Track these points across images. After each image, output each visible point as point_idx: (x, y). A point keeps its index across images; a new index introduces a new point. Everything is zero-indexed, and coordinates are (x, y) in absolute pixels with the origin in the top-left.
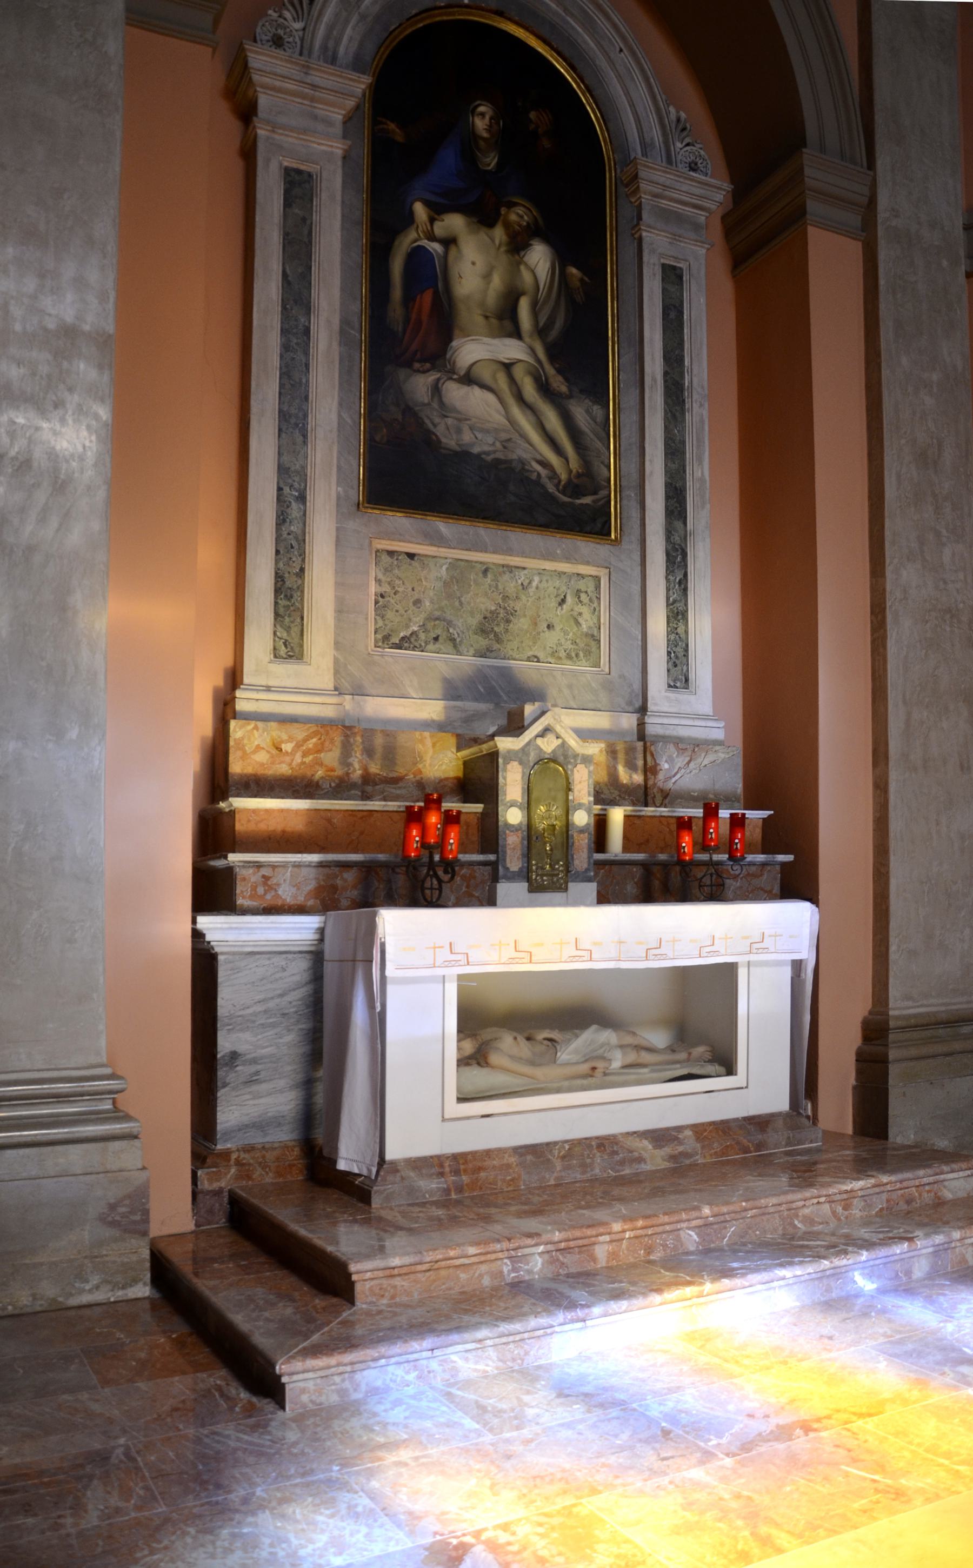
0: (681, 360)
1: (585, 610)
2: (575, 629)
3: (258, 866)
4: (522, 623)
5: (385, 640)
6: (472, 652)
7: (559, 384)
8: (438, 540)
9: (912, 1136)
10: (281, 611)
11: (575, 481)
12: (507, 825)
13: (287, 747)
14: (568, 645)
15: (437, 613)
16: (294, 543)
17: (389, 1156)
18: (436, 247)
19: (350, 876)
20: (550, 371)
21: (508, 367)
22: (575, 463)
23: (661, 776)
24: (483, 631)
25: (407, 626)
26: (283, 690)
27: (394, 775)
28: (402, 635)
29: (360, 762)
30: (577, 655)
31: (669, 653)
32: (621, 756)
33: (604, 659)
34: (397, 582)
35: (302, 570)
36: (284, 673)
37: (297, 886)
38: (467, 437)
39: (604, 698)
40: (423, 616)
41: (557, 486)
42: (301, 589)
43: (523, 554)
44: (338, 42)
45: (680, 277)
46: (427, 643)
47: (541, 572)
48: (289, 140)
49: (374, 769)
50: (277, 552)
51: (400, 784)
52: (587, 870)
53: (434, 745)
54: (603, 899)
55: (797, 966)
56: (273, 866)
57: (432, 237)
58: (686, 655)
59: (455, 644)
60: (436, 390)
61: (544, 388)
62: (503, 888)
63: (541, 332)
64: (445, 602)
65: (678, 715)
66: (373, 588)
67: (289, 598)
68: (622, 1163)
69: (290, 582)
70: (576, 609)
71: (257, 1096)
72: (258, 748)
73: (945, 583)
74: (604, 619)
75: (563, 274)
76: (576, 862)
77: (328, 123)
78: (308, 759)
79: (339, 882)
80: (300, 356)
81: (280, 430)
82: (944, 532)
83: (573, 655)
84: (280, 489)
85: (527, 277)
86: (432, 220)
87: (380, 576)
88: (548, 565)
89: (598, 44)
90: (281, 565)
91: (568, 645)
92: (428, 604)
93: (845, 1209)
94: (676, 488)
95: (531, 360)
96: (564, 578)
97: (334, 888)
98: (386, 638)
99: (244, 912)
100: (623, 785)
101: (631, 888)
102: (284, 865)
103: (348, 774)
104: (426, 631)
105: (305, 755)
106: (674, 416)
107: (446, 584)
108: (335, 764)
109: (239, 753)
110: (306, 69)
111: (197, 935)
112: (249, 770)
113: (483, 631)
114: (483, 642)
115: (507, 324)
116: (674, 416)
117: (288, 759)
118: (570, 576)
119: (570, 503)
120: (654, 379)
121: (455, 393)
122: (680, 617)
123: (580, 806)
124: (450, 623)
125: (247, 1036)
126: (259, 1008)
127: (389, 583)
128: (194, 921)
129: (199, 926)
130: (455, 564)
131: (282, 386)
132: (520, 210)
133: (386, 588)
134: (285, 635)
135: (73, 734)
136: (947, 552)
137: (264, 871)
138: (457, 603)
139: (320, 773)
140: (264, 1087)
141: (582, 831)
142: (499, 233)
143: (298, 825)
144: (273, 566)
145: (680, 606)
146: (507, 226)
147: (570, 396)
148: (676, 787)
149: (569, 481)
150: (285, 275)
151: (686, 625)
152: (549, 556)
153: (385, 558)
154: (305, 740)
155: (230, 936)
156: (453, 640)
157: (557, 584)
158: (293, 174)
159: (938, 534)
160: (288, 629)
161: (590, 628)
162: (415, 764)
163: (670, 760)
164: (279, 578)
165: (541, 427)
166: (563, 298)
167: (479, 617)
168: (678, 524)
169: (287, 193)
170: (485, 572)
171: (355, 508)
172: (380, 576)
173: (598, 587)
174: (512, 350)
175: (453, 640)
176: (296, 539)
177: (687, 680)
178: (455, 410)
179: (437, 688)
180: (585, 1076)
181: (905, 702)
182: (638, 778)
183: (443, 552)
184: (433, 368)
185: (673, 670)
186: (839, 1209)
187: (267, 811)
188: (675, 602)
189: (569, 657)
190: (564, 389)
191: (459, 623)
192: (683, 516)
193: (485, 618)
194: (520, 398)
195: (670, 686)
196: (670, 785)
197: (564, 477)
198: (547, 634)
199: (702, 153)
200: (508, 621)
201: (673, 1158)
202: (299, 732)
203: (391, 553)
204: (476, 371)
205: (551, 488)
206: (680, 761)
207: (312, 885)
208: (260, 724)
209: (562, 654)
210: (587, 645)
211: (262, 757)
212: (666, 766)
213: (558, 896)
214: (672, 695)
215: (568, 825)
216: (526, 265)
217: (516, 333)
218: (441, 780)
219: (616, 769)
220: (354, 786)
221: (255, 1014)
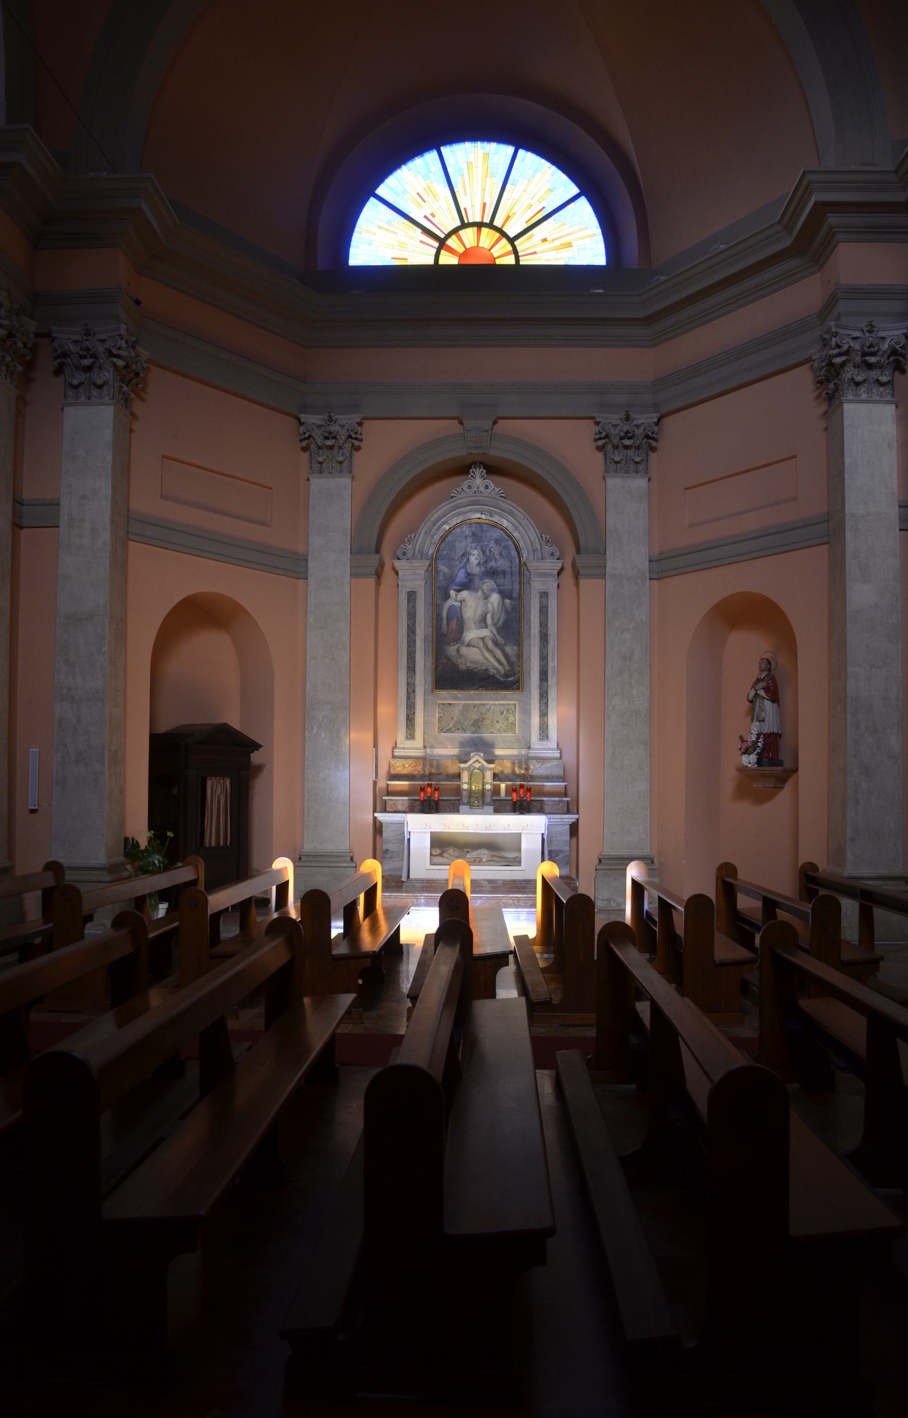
1: (511, 716)
2: (507, 722)
3: (392, 800)
4: (488, 722)
5: (441, 730)
6: (470, 732)
7: (501, 640)
8: (458, 699)
9: (606, 896)
10: (408, 725)
11: (507, 673)
12: (463, 789)
13: (406, 766)
14: (504, 727)
15: (458, 721)
16: (412, 705)
17: (411, 877)
19: (418, 803)
20: (498, 637)
21: (483, 639)
22: (507, 667)
23: (530, 771)
24: (474, 725)
25: (449, 726)
26: (408, 749)
27: (439, 772)
28: (447, 728)
29: (429, 769)
30: (507, 730)
31: (540, 728)
32: (517, 764)
34: (445, 713)
35: (414, 713)
36: (409, 744)
40: (454, 722)
41: (500, 676)
42: (414, 718)
43: (486, 700)
44: (424, 547)
45: (548, 595)
46: (455, 730)
47: (494, 705)
49: (433, 771)
50: (407, 708)
51: (441, 775)
52: (490, 802)
53: (452, 763)
55: (543, 834)
56: (396, 800)
58: (547, 728)
59: (464, 730)
60: (458, 650)
61: (496, 643)
62: (461, 808)
63: (495, 625)
64: (461, 718)
65: (543, 749)
66: (437, 715)
67: (410, 721)
68: (476, 886)
69: (411, 716)
70: (507, 715)
72: (398, 766)
73: (633, 702)
75: (503, 604)
76: (486, 800)
78: (413, 769)
79: (415, 805)
80: (413, 649)
81: (407, 672)
83: (506, 730)
84: (407, 690)
85: (490, 606)
87: (440, 711)
88: (497, 702)
90: (408, 712)
91: (504, 727)
92: (455, 718)
93: (518, 902)
94: (544, 671)
95: (491, 635)
96: (503, 706)
97: (414, 806)
98: (442, 730)
99: (388, 812)
100: (517, 774)
101: (508, 808)
102: (399, 800)
103: (424, 773)
104: (455, 727)
105: (411, 768)
106: (544, 646)
107: (461, 712)
108: (421, 770)
109: (393, 768)
110: (411, 563)
111: (375, 819)
112: (396, 772)
113: (474, 725)
114: (474, 729)
115: (483, 624)
116: (544, 646)
117: (406, 769)
118: (505, 705)
119: (504, 681)
120: (535, 634)
121: (464, 650)
122: (545, 715)
123: (488, 783)
124: (463, 724)
125: (390, 845)
126: (394, 838)
127: (443, 713)
128: (373, 815)
129: (375, 816)
130: (464, 705)
131: (408, 658)
133: (442, 715)
134: (409, 732)
135: (341, 768)
136: (635, 691)
137: (394, 801)
138: (465, 718)
139: (416, 773)
141: (488, 790)
143: (406, 788)
144: (406, 712)
145: (545, 712)
147: (506, 645)
148: (535, 774)
150: (408, 625)
151: (548, 718)
153: (441, 706)
154: (412, 763)
155: (384, 818)
156: (463, 729)
157: (500, 708)
158: (410, 593)
160: (410, 730)
161: (512, 721)
162: (445, 769)
163: (534, 765)
164: (408, 715)
165: (495, 657)
166: (503, 612)
167: (472, 721)
170: (475, 706)
171: (431, 692)
172: (440, 711)
173: (515, 707)
174: (485, 633)
175: (463, 729)
176: (413, 704)
177: (547, 736)
179: (457, 745)
180: (473, 862)
182: (523, 772)
183: (460, 702)
184: (457, 643)
185: (542, 734)
186: (516, 902)
187: (398, 785)
188: (543, 710)
189: (505, 731)
190: (503, 642)
191: (466, 723)
192: (547, 680)
193: (475, 721)
195: (540, 739)
196: (534, 773)
199: (555, 548)
200: (483, 721)
201: (493, 887)
202: (410, 761)
203: (443, 704)
205: (498, 677)
206: (538, 766)
207: (407, 805)
208: (399, 760)
209: (502, 730)
210: (511, 727)
211: (399, 769)
212: (533, 767)
213: (480, 811)
215: (483, 789)
216: (490, 603)
217: (486, 627)
218: (454, 774)
219: (514, 768)
220: (426, 776)
221: (392, 839)
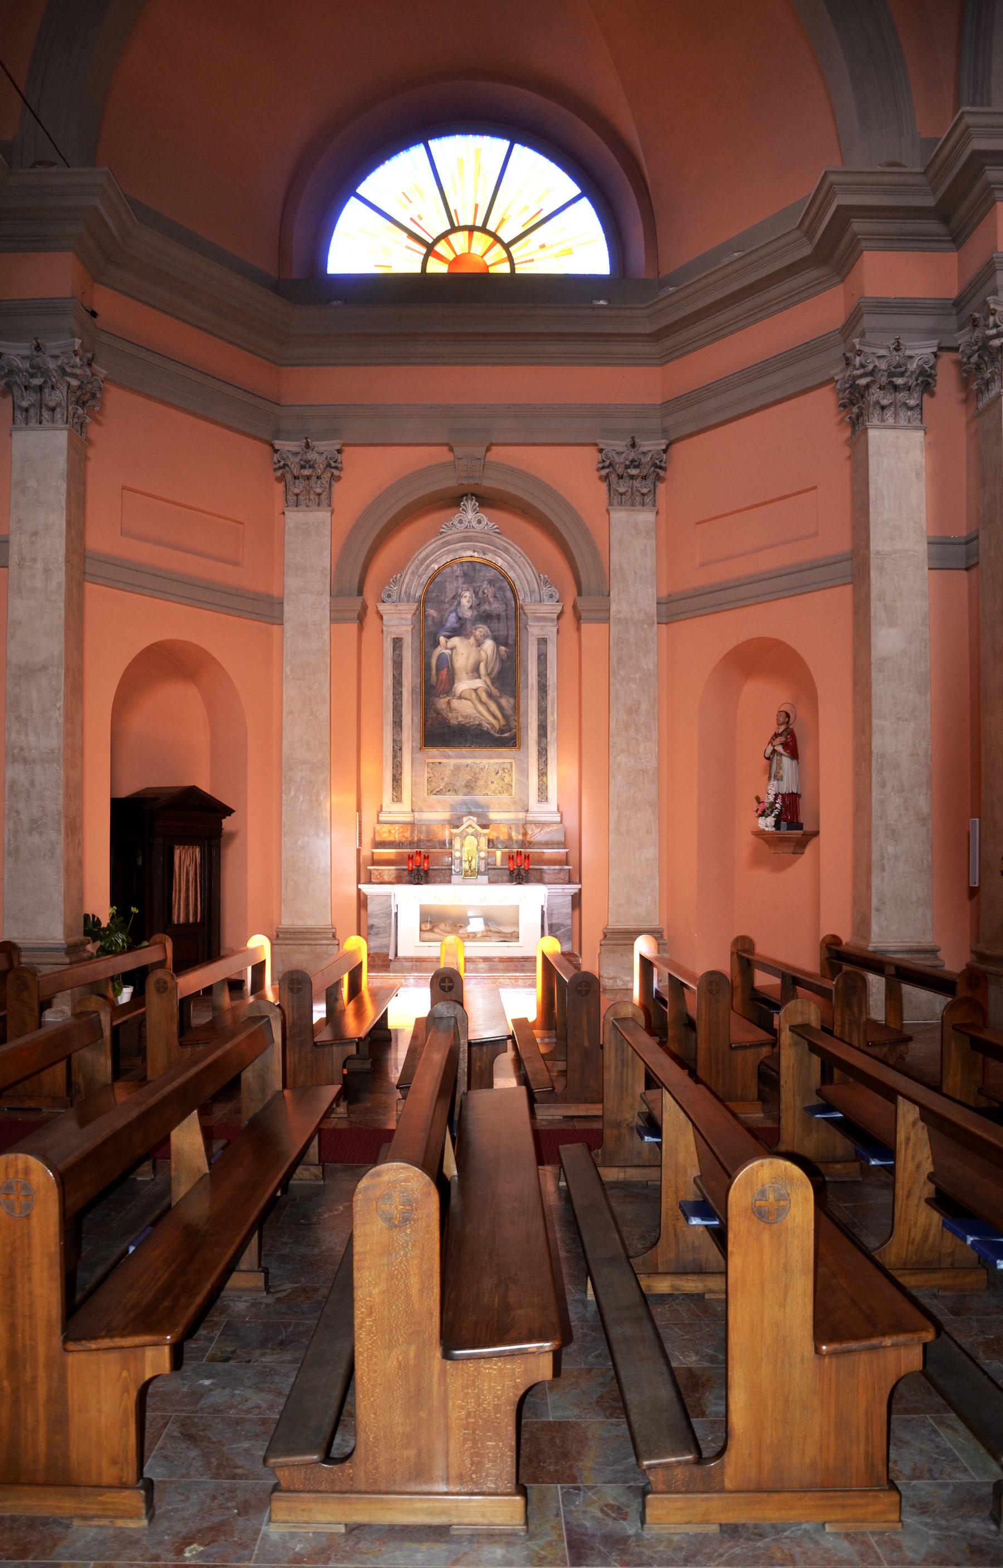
0: (546, 675)
1: (507, 776)
3: (378, 870)
4: (481, 783)
5: (431, 792)
7: (495, 692)
13: (393, 832)
14: (500, 789)
18: (448, 652)
19: (406, 873)
20: (492, 688)
21: (475, 690)
22: (502, 722)
23: (528, 836)
24: (466, 786)
33: (513, 793)
36: (396, 807)
37: (390, 876)
38: (460, 719)
39: (512, 807)
42: (401, 779)
44: (410, 588)
45: (546, 642)
48: (394, 629)
54: (491, 882)
55: (542, 907)
57: (447, 648)
60: (449, 703)
61: (490, 695)
63: (489, 675)
65: (541, 812)
66: (426, 775)
71: (379, 938)
74: (514, 778)
75: (498, 651)
77: (406, 619)
80: (399, 702)
82: (641, 739)
85: (483, 654)
86: (447, 642)
89: (511, 558)
91: (500, 789)
95: (485, 686)
99: (374, 883)
111: (359, 891)
112: (382, 839)
113: (466, 786)
114: (466, 790)
115: (476, 675)
121: (455, 703)
124: (454, 785)
125: (376, 920)
132: (480, 629)
133: (431, 775)
136: (641, 748)
140: (381, 935)
142: (472, 640)
143: (393, 857)
146: (475, 637)
147: (501, 697)
149: (500, 728)
150: (394, 675)
152: (490, 758)
159: (637, 740)
163: (532, 830)
164: (394, 776)
167: (465, 782)
168: (544, 740)
169: (394, 646)
173: (512, 766)
174: (478, 683)
178: (455, 710)
181: (617, 808)
182: (520, 837)
189: (500, 793)
192: (546, 736)
194: (481, 701)
196: (532, 839)
197: (498, 727)
198: (492, 785)
202: (397, 827)
203: (433, 763)
204: (463, 695)
205: (492, 732)
206: (537, 831)
207: (394, 876)
211: (385, 835)
214: (539, 805)
217: (479, 677)
